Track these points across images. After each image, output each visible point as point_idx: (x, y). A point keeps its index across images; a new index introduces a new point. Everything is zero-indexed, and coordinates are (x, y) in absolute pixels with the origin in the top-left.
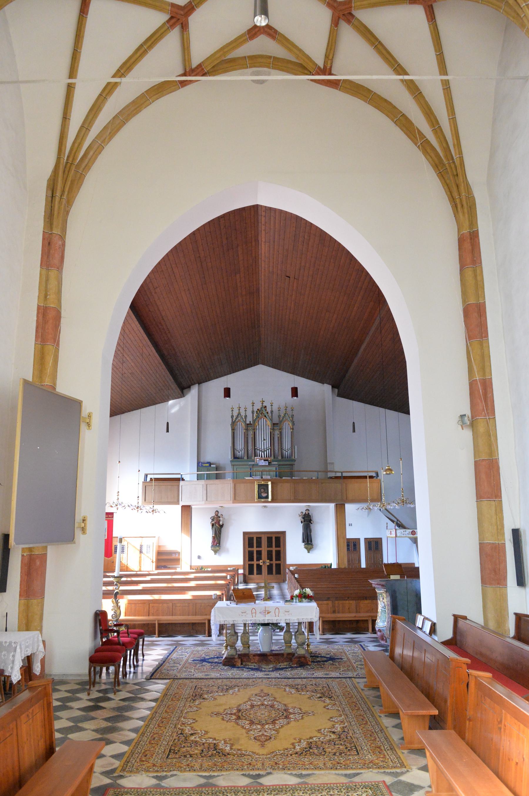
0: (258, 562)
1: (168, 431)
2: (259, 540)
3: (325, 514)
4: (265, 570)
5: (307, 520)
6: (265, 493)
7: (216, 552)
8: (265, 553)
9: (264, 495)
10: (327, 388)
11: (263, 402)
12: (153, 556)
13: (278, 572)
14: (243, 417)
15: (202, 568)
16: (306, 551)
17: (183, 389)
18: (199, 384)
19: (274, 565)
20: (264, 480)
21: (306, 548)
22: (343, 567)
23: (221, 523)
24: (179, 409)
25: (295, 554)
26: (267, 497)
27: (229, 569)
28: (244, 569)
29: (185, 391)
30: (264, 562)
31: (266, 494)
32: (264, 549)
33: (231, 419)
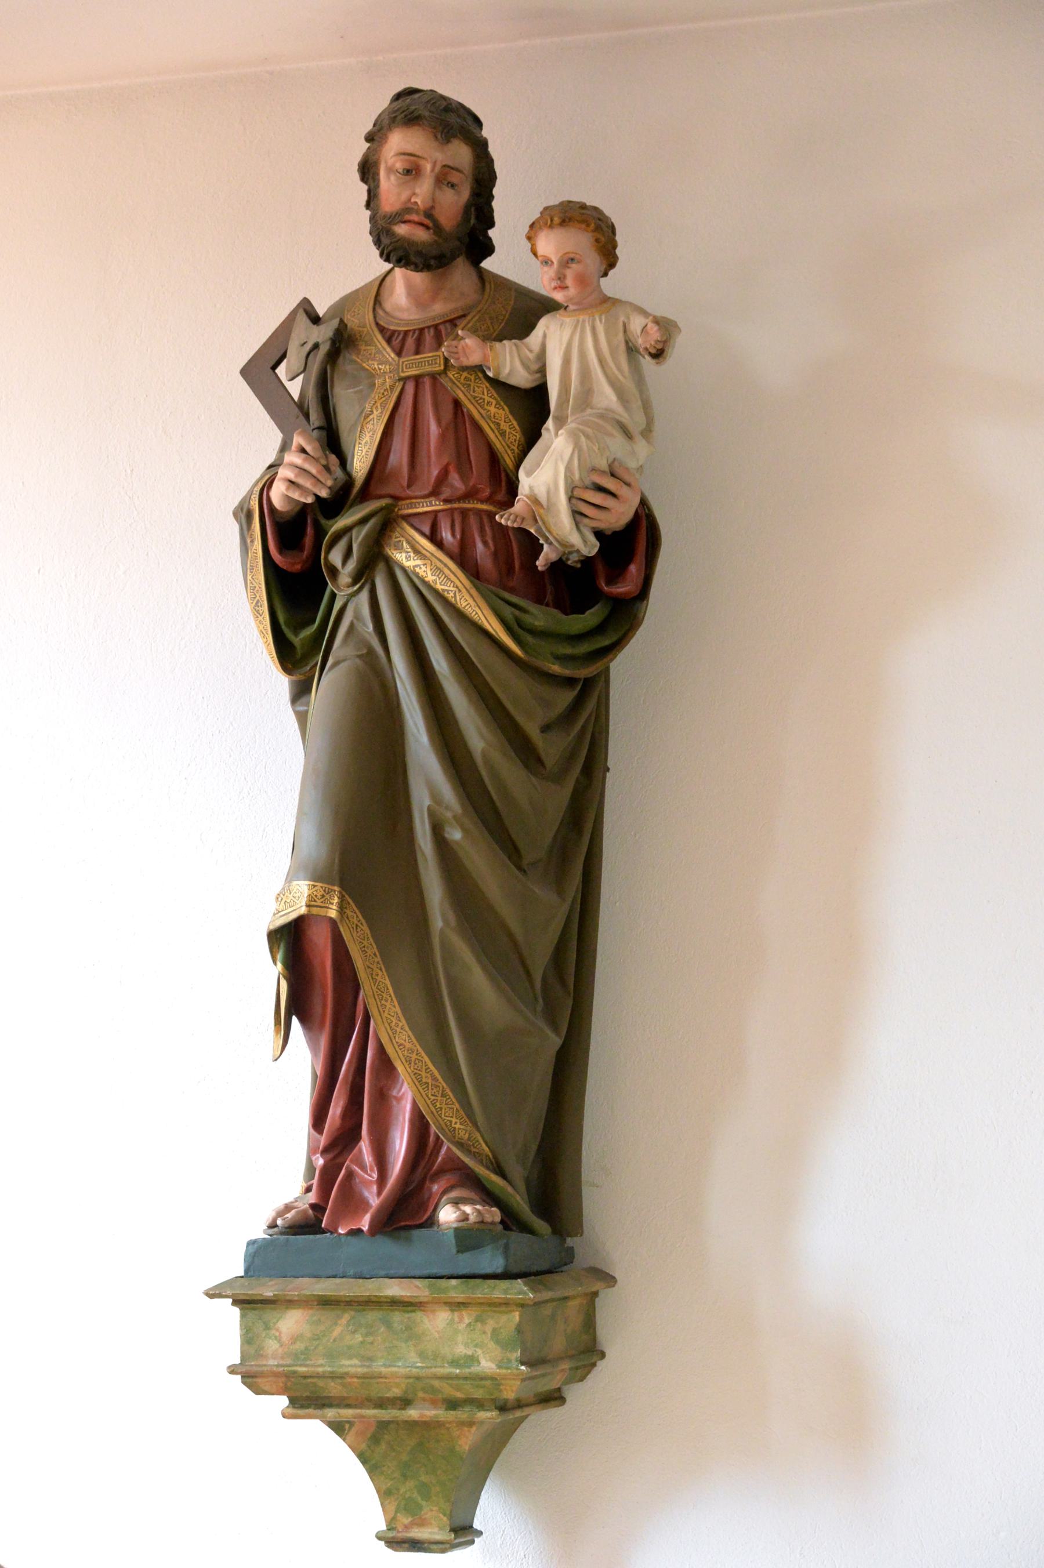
23: (547, 476)
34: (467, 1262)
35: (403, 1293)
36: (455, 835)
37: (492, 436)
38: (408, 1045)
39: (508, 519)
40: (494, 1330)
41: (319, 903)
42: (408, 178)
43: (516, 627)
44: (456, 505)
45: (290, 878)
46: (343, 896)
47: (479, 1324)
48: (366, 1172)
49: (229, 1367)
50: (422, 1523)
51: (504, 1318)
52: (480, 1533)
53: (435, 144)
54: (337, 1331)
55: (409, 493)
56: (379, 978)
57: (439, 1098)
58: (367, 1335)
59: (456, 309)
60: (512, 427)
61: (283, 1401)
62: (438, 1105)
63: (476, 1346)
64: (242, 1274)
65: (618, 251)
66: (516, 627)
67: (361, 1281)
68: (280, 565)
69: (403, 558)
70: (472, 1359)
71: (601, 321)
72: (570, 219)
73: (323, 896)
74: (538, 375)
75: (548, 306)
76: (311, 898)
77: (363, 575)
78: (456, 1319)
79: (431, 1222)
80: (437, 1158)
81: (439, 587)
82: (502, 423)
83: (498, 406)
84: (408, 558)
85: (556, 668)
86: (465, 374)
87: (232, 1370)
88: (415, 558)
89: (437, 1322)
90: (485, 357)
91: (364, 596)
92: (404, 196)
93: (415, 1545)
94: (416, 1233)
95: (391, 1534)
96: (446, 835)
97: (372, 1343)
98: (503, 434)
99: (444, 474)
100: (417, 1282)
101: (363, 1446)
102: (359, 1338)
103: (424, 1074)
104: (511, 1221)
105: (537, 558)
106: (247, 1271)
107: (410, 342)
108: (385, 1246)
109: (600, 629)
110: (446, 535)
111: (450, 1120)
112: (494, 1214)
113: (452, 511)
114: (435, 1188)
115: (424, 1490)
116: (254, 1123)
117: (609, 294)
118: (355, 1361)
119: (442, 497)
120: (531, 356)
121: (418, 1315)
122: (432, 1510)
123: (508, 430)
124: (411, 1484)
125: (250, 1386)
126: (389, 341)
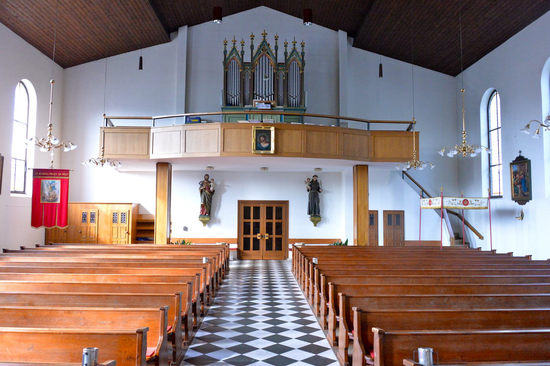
0: (255, 236)
1: (141, 68)
2: (257, 210)
3: (337, 173)
4: (263, 245)
5: (315, 188)
6: (266, 142)
7: (205, 223)
8: (263, 226)
9: (264, 145)
10: (342, 35)
11: (265, 35)
12: (128, 225)
13: (279, 247)
14: (240, 53)
15: (184, 242)
16: (312, 224)
17: (168, 32)
18: (189, 26)
19: (274, 240)
20: (264, 125)
21: (313, 221)
22: (363, 245)
23: (211, 189)
24: (167, 57)
25: (299, 227)
26: (269, 148)
27: (217, 244)
28: (238, 243)
29: (172, 34)
30: (263, 236)
31: (267, 144)
32: (263, 221)
33: (223, 55)
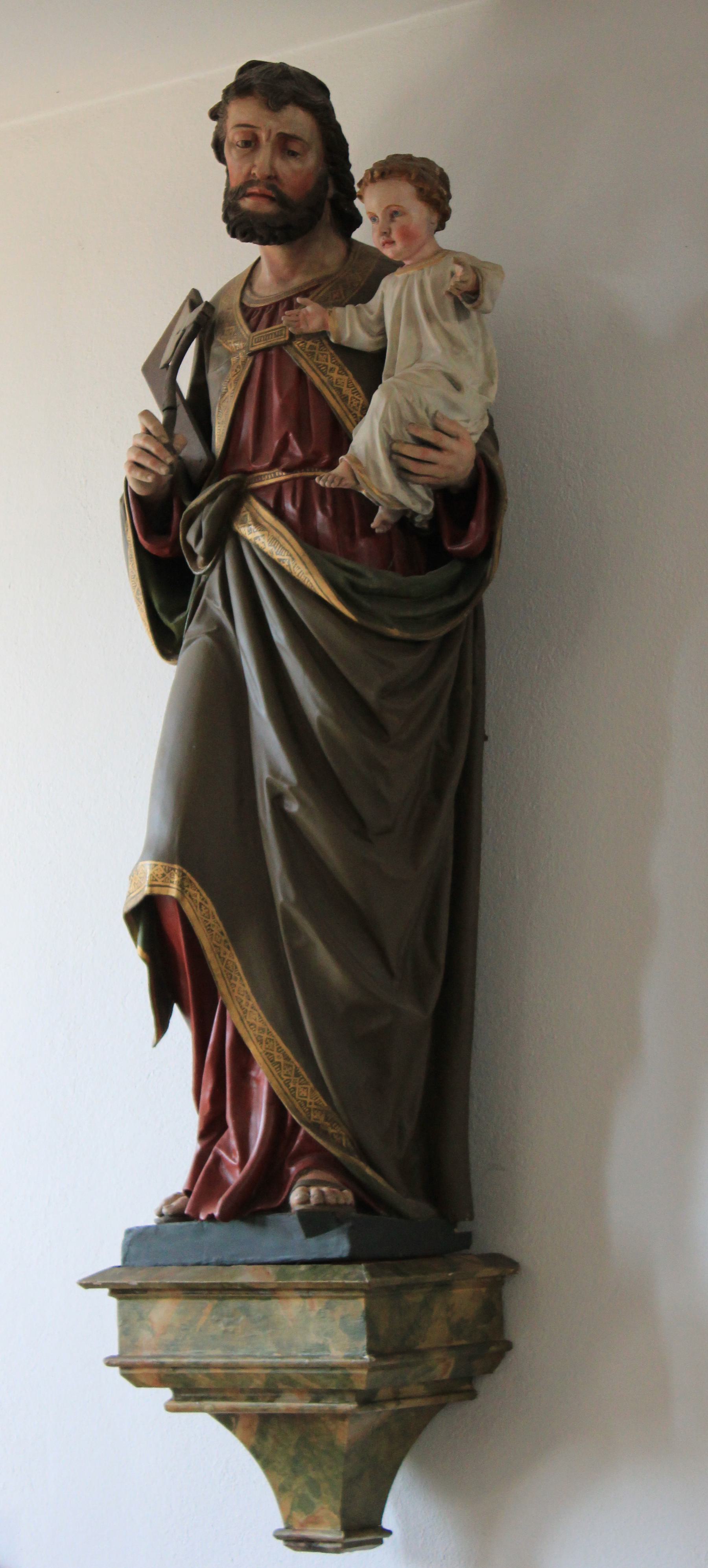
34: (314, 1247)
35: (256, 1281)
36: (293, 807)
37: (332, 402)
38: (259, 1024)
39: (326, 480)
40: (343, 1318)
41: (160, 882)
42: (248, 150)
43: (349, 590)
44: (297, 475)
45: (142, 858)
46: (184, 874)
47: (328, 1311)
48: (230, 1157)
49: (107, 1358)
50: (315, 1521)
51: (351, 1303)
52: (389, 1533)
53: (266, 113)
54: (203, 1319)
55: (257, 467)
56: (227, 957)
57: (292, 1078)
58: (228, 1324)
59: (312, 281)
60: (355, 392)
61: (166, 1393)
62: (292, 1085)
63: (326, 1334)
64: (119, 1263)
65: (452, 204)
66: (349, 590)
67: (220, 1268)
68: (154, 553)
69: (248, 532)
70: (323, 1347)
71: (429, 273)
72: (391, 172)
73: (164, 875)
74: (380, 338)
75: (390, 266)
76: (153, 878)
77: (214, 552)
78: (308, 1307)
79: (285, 1207)
80: (295, 1141)
81: (276, 557)
82: (345, 388)
83: (342, 372)
84: (250, 532)
85: (395, 632)
86: (309, 343)
87: (110, 1362)
88: (262, 534)
89: (290, 1310)
90: (325, 324)
91: (216, 573)
92: (245, 170)
93: (311, 1545)
94: (271, 1217)
95: (287, 1533)
96: (286, 808)
97: (233, 1332)
98: (345, 399)
99: (285, 443)
100: (270, 1269)
101: (253, 1440)
102: (221, 1326)
103: (275, 1054)
104: (368, 1201)
105: (372, 521)
106: (125, 1259)
107: (265, 318)
108: (240, 1231)
109: (452, 588)
110: (289, 507)
111: (304, 1098)
112: (347, 1196)
113: (294, 480)
114: (293, 1170)
115: (314, 1485)
116: (136, 1114)
117: (444, 247)
118: (218, 1352)
119: (282, 467)
120: (372, 317)
121: (274, 1304)
122: (323, 1508)
123: (350, 395)
124: (301, 1480)
125: (130, 1378)
126: (247, 320)
